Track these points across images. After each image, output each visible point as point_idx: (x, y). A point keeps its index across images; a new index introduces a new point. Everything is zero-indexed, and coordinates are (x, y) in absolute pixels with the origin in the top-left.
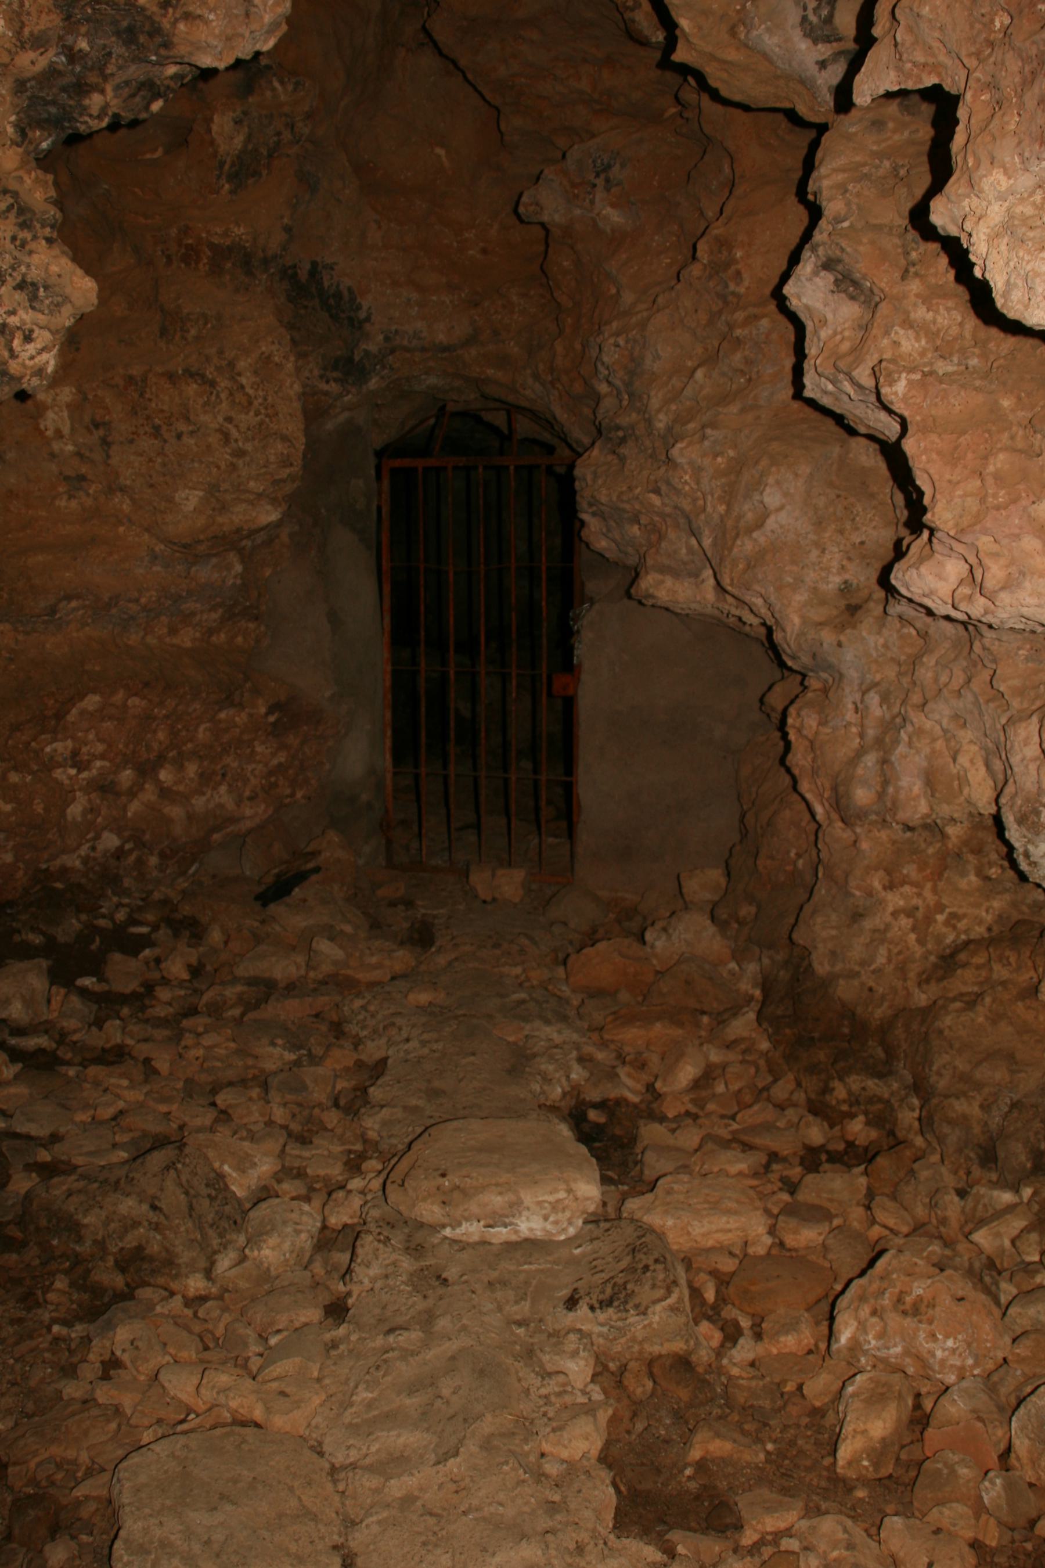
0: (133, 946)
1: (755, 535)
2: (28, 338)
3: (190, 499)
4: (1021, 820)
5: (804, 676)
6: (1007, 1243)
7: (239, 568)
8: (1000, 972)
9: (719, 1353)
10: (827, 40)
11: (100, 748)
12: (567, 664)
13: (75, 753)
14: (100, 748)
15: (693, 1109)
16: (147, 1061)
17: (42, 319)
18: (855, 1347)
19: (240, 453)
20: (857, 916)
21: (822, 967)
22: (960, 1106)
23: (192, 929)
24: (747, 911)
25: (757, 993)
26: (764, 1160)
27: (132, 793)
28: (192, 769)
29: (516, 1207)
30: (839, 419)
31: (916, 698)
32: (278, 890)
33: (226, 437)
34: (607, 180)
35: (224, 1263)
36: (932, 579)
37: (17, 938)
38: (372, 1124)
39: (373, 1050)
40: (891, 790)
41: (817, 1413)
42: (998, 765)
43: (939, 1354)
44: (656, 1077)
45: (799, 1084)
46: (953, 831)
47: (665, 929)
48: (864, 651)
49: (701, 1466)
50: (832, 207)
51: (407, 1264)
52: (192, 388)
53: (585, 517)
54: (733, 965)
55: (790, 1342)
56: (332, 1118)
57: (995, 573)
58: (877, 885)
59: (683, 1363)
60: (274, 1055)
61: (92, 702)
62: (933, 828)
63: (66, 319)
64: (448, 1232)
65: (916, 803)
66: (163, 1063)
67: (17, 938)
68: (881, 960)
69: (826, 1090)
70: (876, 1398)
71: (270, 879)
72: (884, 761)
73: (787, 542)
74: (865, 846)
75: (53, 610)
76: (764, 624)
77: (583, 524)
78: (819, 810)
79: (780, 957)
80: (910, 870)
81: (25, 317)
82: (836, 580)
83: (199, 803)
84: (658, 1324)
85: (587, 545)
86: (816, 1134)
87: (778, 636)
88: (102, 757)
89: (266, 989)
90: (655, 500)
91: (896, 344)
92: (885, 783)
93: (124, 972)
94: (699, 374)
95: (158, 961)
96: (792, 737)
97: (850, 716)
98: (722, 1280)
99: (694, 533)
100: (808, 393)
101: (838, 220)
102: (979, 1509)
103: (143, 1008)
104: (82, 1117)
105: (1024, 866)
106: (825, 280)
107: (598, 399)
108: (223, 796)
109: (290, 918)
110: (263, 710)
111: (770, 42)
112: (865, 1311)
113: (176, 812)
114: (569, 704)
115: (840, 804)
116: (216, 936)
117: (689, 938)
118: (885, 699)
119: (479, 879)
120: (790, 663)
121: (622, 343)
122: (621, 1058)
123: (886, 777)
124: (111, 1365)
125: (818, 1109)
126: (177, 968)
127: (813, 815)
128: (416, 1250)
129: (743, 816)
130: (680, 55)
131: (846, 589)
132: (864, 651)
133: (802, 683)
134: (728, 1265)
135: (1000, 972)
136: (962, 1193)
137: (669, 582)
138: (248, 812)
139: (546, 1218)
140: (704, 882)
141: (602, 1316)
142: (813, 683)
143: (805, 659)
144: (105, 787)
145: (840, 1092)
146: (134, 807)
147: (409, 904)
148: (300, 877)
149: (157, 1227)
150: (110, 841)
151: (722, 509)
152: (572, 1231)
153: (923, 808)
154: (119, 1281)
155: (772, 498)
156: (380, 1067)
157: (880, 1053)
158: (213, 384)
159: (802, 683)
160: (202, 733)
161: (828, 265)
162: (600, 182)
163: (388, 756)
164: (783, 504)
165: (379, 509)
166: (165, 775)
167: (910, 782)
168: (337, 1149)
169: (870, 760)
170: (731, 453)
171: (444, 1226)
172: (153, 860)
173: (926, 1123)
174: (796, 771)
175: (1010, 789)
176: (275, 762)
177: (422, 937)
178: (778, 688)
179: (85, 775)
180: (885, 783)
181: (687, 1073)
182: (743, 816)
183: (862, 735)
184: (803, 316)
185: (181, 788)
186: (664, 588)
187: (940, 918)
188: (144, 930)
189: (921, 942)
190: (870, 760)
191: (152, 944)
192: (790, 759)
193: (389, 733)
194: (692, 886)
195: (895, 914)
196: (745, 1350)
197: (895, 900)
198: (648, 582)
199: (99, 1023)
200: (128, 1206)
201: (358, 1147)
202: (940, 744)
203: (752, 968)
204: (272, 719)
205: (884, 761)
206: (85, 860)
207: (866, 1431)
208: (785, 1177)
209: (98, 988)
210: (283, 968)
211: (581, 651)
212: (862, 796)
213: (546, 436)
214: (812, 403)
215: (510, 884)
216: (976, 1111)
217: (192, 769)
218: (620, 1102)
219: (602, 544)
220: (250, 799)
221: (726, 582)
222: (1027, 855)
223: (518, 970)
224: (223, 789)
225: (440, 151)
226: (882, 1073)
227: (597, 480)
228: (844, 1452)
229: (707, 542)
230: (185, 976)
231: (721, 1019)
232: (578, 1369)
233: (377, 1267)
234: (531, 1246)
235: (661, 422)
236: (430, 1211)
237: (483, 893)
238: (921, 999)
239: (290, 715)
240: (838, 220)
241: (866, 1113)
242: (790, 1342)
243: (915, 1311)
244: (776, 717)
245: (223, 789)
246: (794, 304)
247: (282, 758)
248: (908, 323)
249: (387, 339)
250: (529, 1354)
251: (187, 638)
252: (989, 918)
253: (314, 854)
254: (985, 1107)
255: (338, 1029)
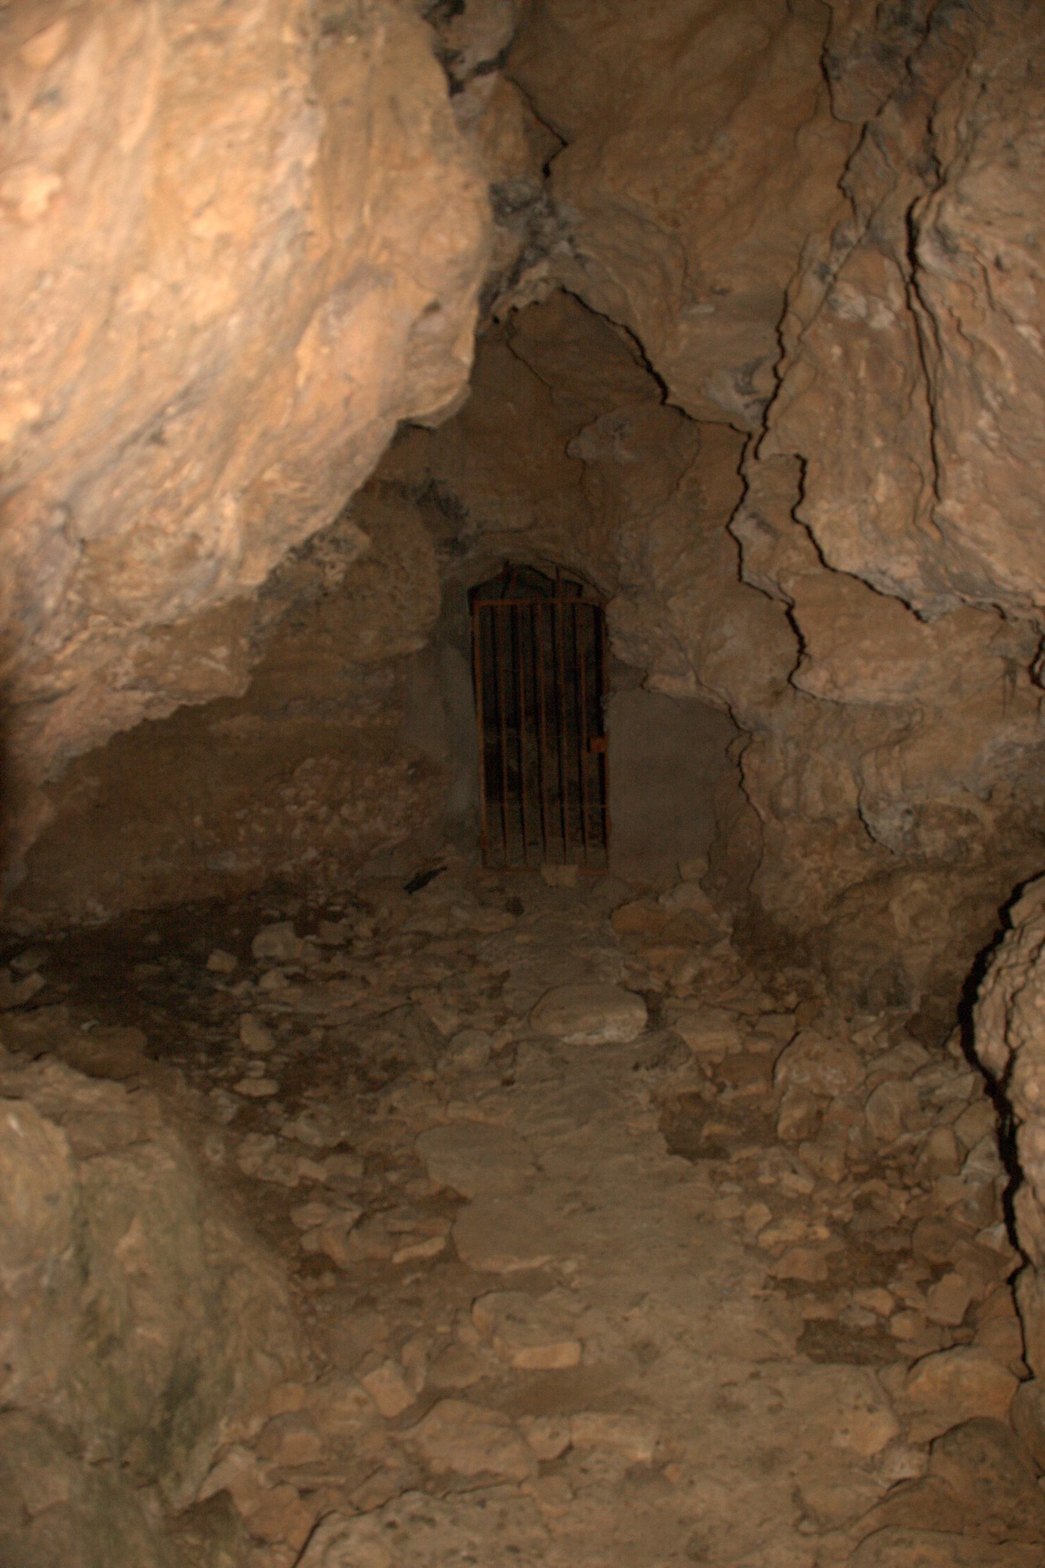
0: (336, 917)
1: (719, 652)
2: (333, 567)
3: (369, 636)
4: (870, 808)
5: (751, 735)
6: (871, 1039)
7: (392, 676)
8: (869, 900)
9: (715, 1096)
10: (749, 393)
11: (312, 792)
12: (601, 732)
13: (297, 795)
14: (312, 792)
15: (693, 992)
16: (363, 979)
17: (341, 557)
18: (787, 1080)
19: (402, 608)
20: (786, 875)
21: (768, 906)
22: (847, 975)
23: (368, 908)
24: (721, 881)
25: (730, 930)
26: (736, 1015)
27: (326, 822)
28: (361, 806)
29: (602, 1024)
30: (765, 593)
31: (814, 744)
32: (419, 883)
33: (393, 598)
34: (621, 434)
35: (441, 1065)
36: (814, 680)
37: (264, 913)
38: (509, 1000)
39: (498, 968)
40: (802, 798)
41: (767, 1117)
42: (859, 781)
43: (829, 1078)
44: (671, 977)
45: (756, 978)
46: (841, 822)
47: (671, 895)
48: (783, 718)
49: (708, 1138)
50: (754, 485)
51: (545, 1055)
52: (371, 569)
53: (613, 639)
54: (715, 916)
55: (753, 1088)
56: (483, 1001)
57: (842, 677)
58: (797, 855)
59: (696, 1097)
60: (439, 972)
61: (309, 763)
62: (828, 820)
63: (354, 556)
64: (566, 1040)
65: (817, 806)
66: (373, 979)
67: (264, 913)
68: (802, 899)
69: (772, 979)
70: (796, 1101)
71: (412, 876)
72: (798, 782)
73: (740, 658)
74: (790, 832)
75: (286, 707)
76: (726, 703)
77: (612, 643)
78: (762, 813)
79: (742, 905)
80: (816, 845)
81: (332, 557)
82: (767, 677)
83: (365, 827)
84: (680, 1078)
85: (614, 656)
86: (767, 1003)
87: (734, 711)
88: (313, 798)
89: (427, 937)
90: (658, 631)
91: (789, 558)
92: (799, 794)
93: (332, 932)
94: (683, 556)
95: (351, 927)
96: (745, 770)
97: (778, 756)
98: (714, 1066)
99: (682, 650)
100: (746, 579)
101: (757, 491)
102: (848, 1141)
103: (348, 953)
104: (336, 1005)
105: (873, 834)
106: (752, 523)
107: (619, 566)
108: (379, 824)
109: (430, 898)
110: (405, 766)
111: (720, 396)
112: (790, 1061)
113: (352, 833)
114: (602, 757)
115: (774, 808)
116: (384, 912)
117: (688, 898)
118: (798, 746)
119: (548, 873)
120: (742, 726)
121: (634, 535)
122: (649, 968)
123: (799, 789)
124: (392, 1110)
125: (769, 990)
126: (364, 929)
127: (759, 816)
128: (550, 1050)
129: (717, 823)
130: (670, 401)
131: (773, 682)
132: (783, 718)
133: (750, 737)
134: (718, 1059)
135: (869, 900)
136: (848, 1020)
137: (667, 679)
138: (395, 834)
139: (619, 1029)
140: (695, 867)
141: (653, 1072)
142: (757, 738)
143: (751, 724)
144: (311, 818)
145: (781, 979)
146: (328, 830)
147: (502, 890)
148: (432, 874)
149: (403, 1045)
150: (312, 853)
151: (699, 637)
152: (633, 1037)
153: (821, 807)
154: (385, 1076)
155: (727, 630)
156: (507, 975)
157: (803, 954)
158: (385, 566)
159: (750, 737)
160: (368, 782)
161: (753, 516)
162: (617, 435)
163: (483, 795)
164: (735, 634)
165: (473, 633)
166: (345, 811)
167: (813, 794)
168: (489, 1015)
169: (790, 781)
170: (703, 604)
171: (563, 1036)
172: (334, 867)
173: (829, 987)
174: (749, 791)
175: (864, 792)
176: (411, 801)
177: (516, 908)
178: (736, 743)
179: (303, 809)
180: (799, 794)
181: (689, 973)
182: (717, 823)
183: (785, 768)
184: (741, 539)
185: (354, 819)
186: (665, 684)
187: (835, 873)
188: (338, 908)
189: (825, 887)
190: (790, 781)
191: (345, 916)
192: (745, 784)
193: (483, 780)
194: (687, 869)
195: (809, 872)
196: (728, 1095)
197: (808, 863)
198: (654, 680)
199: (328, 960)
200: (386, 1036)
201: (501, 1014)
202: (829, 770)
203: (727, 915)
204: (410, 772)
205: (798, 782)
206: (295, 866)
207: (791, 1117)
208: (747, 1023)
209: (319, 941)
210: (434, 926)
211: (609, 722)
212: (786, 802)
213: (576, 579)
214: (749, 585)
215: (568, 875)
216: (856, 977)
217: (361, 806)
218: (649, 991)
219: (623, 656)
220: (397, 825)
221: (703, 679)
222: (874, 828)
223: (581, 923)
224: (379, 819)
225: (510, 405)
226: (804, 964)
227: (619, 615)
228: (781, 1127)
229: (690, 656)
230: (370, 934)
231: (708, 946)
232: (643, 1098)
233: (528, 1059)
234: (610, 1045)
235: (660, 584)
236: (555, 1028)
237: (550, 881)
238: (826, 920)
239: (422, 770)
240: (757, 491)
241: (797, 990)
242: (753, 1088)
243: (817, 1057)
244: (736, 760)
245: (379, 819)
246: (736, 533)
247: (416, 798)
248: (795, 547)
249: (479, 526)
250: (616, 1090)
251: (358, 722)
252: (864, 872)
253: (440, 859)
254: (862, 974)
255: (474, 960)
